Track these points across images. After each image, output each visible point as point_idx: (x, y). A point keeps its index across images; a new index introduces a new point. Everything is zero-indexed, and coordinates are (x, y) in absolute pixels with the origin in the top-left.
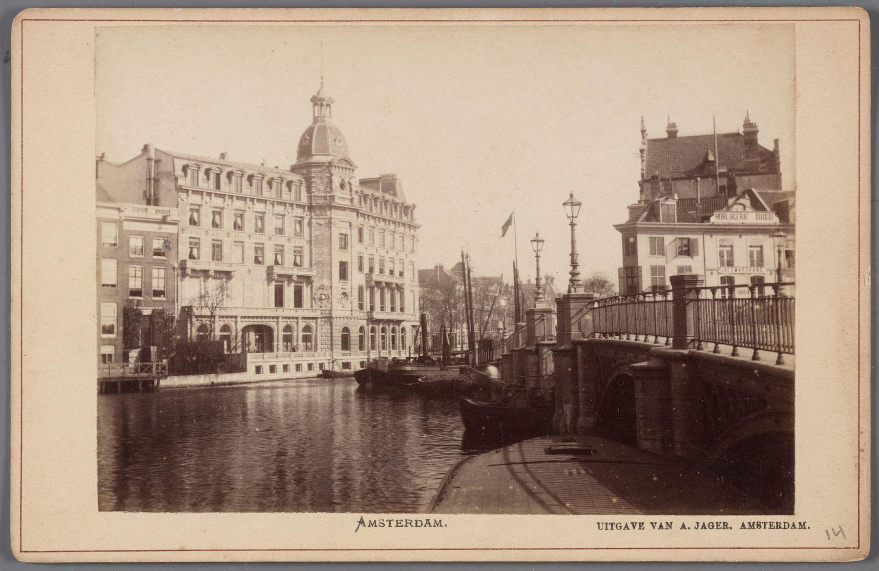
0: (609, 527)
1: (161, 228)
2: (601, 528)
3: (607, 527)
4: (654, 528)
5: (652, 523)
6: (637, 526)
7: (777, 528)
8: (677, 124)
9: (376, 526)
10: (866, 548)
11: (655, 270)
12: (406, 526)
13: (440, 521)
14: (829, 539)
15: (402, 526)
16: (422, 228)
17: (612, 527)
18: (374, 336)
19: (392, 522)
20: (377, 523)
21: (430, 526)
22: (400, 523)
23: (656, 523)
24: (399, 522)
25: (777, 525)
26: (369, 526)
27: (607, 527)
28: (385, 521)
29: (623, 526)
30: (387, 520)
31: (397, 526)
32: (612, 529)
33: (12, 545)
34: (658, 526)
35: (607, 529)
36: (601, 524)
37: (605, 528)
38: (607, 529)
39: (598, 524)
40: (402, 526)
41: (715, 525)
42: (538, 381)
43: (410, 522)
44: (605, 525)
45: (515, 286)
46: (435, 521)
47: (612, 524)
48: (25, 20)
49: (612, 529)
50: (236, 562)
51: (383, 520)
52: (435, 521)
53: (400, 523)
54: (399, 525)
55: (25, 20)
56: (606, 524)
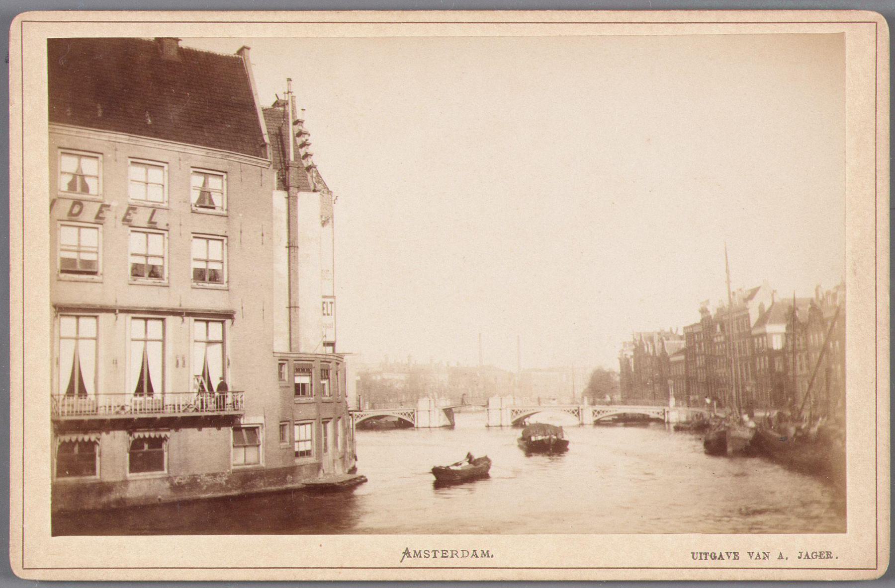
0: (703, 557)
2: (695, 557)
3: (701, 557)
4: (751, 557)
5: (749, 553)
6: (732, 556)
7: (828, 558)
8: (121, 225)
9: (421, 557)
11: (148, 406)
12: (452, 557)
13: (488, 551)
14: (401, 562)
15: (447, 557)
16: (312, 145)
17: (706, 557)
19: (437, 552)
20: (423, 554)
21: (410, 556)
22: (446, 554)
23: (753, 553)
24: (444, 552)
25: (828, 554)
26: (414, 557)
27: (701, 557)
28: (430, 551)
29: (718, 555)
30: (433, 551)
31: (442, 557)
32: (706, 559)
33: (12, 560)
34: (755, 555)
35: (701, 559)
36: (695, 555)
37: (699, 558)
38: (701, 559)
39: (693, 553)
40: (447, 557)
41: (818, 554)
42: (712, 323)
43: (456, 552)
44: (699, 555)
46: (415, 551)
47: (706, 554)
49: (706, 559)
51: (428, 551)
52: (415, 551)
53: (446, 554)
54: (444, 555)
56: (701, 553)
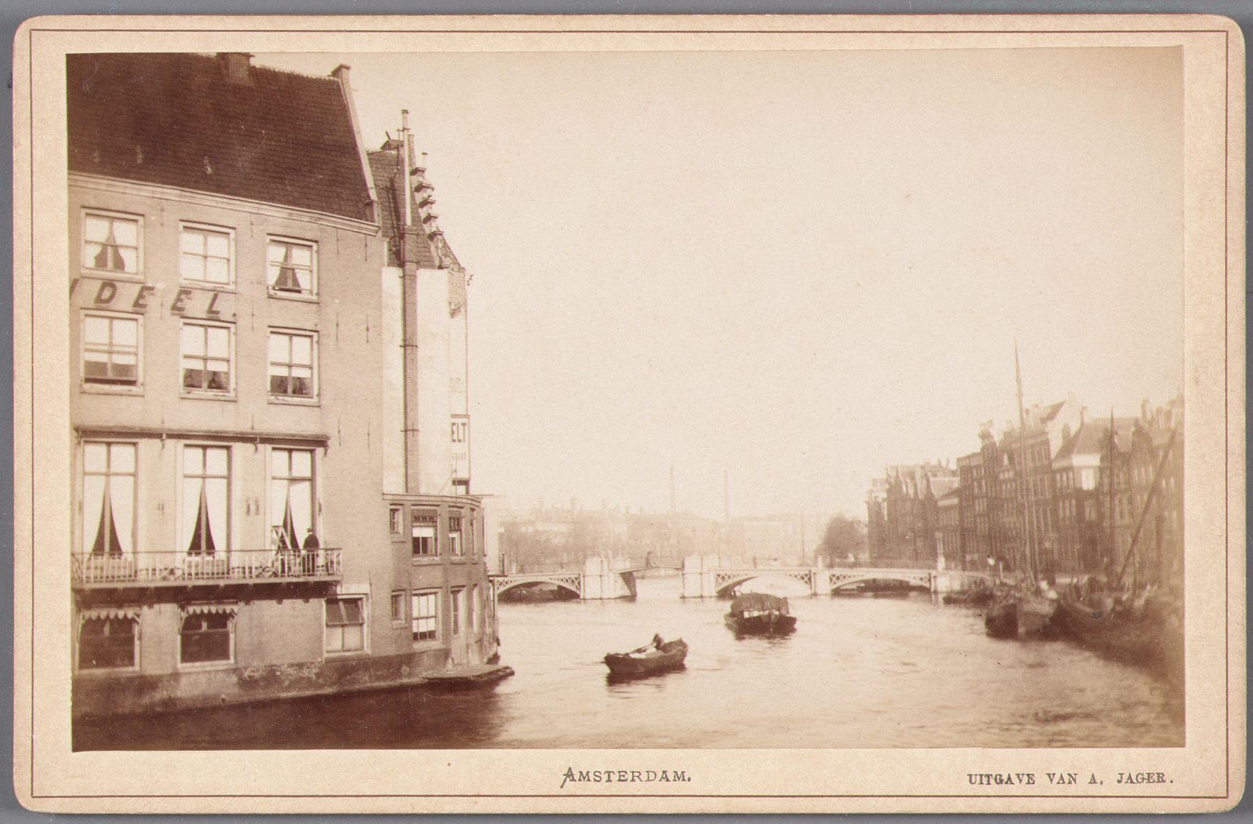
0: (985, 780)
1: (189, 393)
2: (973, 781)
3: (981, 780)
4: (1051, 780)
5: (1049, 775)
6: (1025, 779)
7: (1159, 782)
9: (589, 780)
10: (1236, 796)
12: (633, 780)
13: (683, 772)
14: (562, 787)
15: (626, 780)
17: (989, 781)
18: (261, 439)
19: (611, 774)
20: (592, 776)
21: (573, 780)
22: (624, 776)
23: (1054, 774)
24: (622, 774)
25: (1159, 777)
26: (580, 780)
27: (981, 780)
28: (603, 772)
29: (1005, 778)
30: (606, 772)
31: (619, 780)
32: (989, 783)
34: (1057, 778)
35: (981, 783)
36: (973, 777)
37: (978, 781)
38: (981, 783)
39: (971, 775)
40: (626, 780)
43: (638, 774)
44: (978, 777)
45: (874, 591)
46: (581, 773)
47: (988, 776)
48: (1224, 798)
49: (989, 783)
50: (755, 814)
51: (600, 772)
52: (581, 773)
53: (624, 776)
54: (622, 778)
55: (1224, 798)
56: (981, 775)
